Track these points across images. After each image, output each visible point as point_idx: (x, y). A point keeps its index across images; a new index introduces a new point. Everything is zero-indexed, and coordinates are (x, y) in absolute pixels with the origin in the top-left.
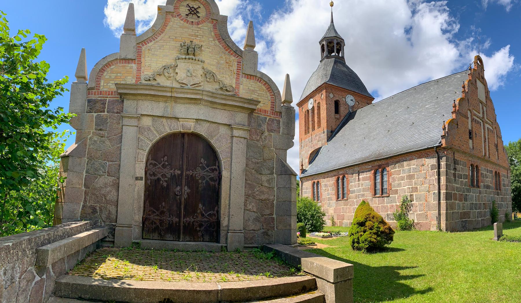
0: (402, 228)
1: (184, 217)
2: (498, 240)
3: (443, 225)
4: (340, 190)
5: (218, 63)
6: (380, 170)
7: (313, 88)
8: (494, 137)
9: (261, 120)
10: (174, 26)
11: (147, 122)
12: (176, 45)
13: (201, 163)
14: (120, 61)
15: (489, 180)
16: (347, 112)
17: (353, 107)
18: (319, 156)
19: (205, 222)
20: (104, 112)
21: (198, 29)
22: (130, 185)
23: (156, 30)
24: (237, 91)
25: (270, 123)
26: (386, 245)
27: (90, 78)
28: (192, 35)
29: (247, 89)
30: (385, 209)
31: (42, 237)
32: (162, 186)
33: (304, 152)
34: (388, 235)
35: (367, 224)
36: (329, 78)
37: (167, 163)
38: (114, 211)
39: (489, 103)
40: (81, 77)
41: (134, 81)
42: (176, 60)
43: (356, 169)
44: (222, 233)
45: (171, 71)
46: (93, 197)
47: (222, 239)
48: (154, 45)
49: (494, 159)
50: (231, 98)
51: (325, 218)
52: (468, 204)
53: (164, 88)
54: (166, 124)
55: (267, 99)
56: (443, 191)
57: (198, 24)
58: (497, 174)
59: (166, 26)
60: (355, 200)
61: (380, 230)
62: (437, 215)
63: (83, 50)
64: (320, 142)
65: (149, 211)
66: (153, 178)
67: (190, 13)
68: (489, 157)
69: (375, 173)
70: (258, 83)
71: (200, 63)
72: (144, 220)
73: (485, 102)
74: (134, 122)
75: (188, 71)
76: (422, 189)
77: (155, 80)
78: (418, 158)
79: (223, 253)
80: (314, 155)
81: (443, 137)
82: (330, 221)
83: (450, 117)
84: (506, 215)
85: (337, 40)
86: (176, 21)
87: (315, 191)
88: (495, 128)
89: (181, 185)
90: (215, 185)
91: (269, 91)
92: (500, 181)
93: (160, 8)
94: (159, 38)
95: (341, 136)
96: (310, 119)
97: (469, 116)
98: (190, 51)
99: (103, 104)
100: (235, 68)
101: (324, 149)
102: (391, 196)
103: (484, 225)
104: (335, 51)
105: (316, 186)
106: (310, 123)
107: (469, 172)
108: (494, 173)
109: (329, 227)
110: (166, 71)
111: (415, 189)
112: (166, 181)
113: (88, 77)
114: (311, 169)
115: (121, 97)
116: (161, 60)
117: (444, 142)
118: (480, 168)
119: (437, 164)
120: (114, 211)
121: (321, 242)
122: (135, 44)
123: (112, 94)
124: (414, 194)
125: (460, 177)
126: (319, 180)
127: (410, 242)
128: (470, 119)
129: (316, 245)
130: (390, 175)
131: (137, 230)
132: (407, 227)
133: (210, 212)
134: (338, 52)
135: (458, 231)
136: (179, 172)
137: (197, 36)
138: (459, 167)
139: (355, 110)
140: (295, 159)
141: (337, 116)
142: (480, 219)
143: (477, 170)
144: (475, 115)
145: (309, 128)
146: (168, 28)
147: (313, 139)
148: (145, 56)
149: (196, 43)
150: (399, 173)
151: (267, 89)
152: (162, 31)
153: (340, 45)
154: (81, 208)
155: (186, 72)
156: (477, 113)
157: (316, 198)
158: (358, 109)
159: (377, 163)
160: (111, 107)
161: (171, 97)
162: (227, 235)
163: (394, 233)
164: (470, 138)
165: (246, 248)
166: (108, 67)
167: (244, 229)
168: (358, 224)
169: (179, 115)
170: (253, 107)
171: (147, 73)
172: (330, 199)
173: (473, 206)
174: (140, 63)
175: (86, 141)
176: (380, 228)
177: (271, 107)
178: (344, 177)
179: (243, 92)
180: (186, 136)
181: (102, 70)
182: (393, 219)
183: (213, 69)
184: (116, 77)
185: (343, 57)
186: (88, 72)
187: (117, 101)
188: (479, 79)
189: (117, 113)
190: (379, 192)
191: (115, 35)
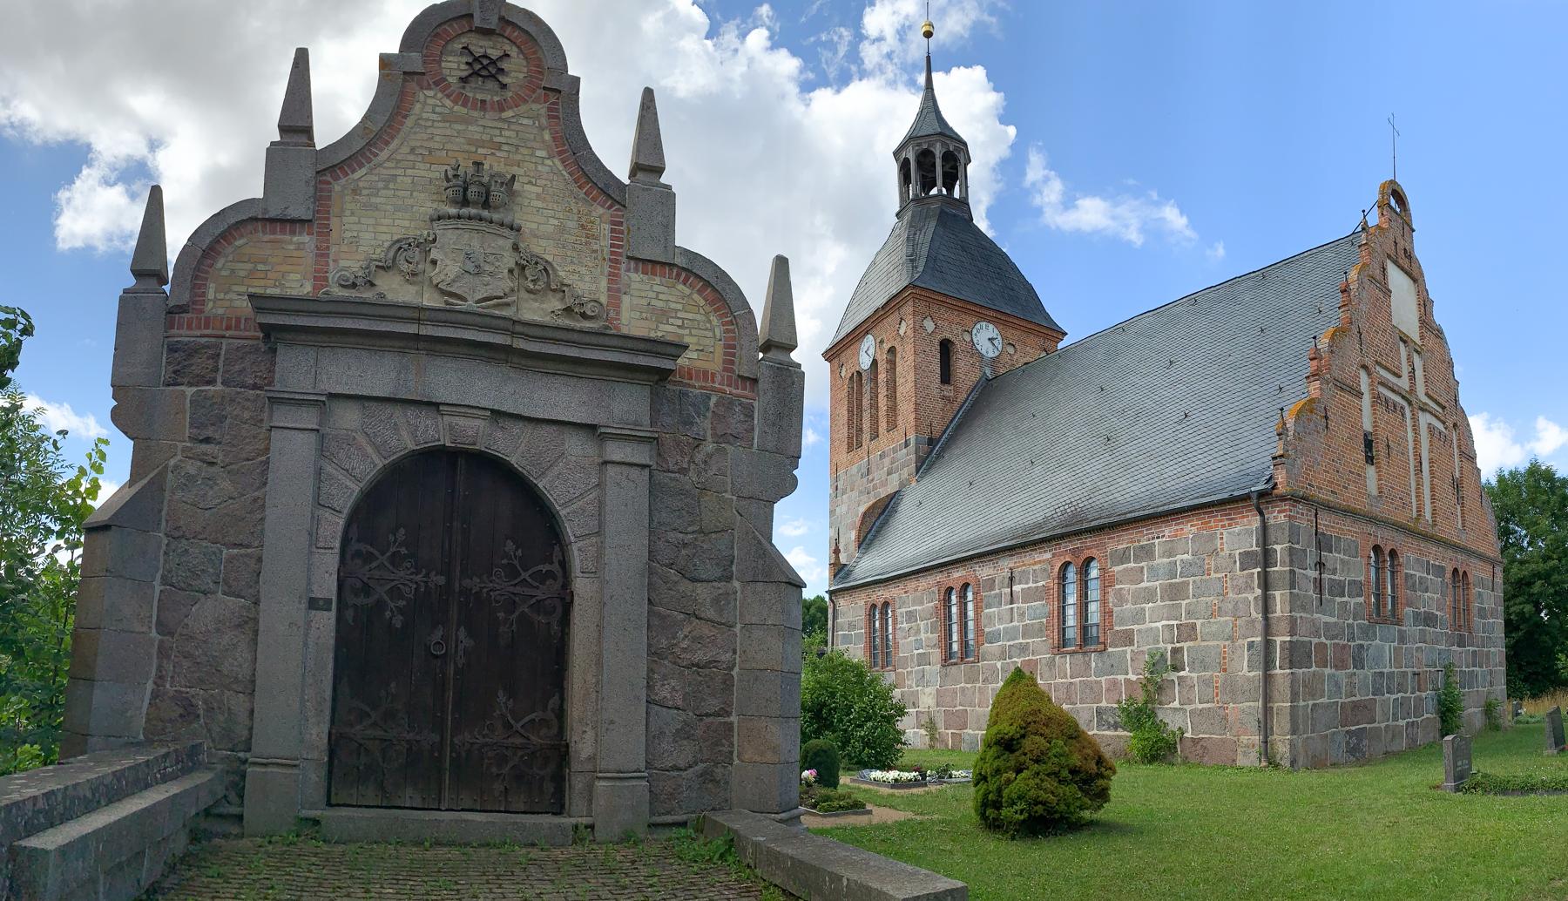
0: (1145, 756)
3: (1282, 746)
5: (562, 229)
8: (1452, 455)
9: (693, 405)
10: (425, 115)
12: (431, 175)
15: (1434, 599)
16: (974, 377)
20: (211, 382)
21: (500, 125)
24: (612, 314)
29: (642, 309)
30: (1093, 691)
31: (29, 805)
33: (844, 508)
34: (1091, 778)
37: (404, 551)
42: (432, 220)
44: (577, 783)
45: (416, 254)
47: (576, 801)
48: (369, 177)
49: (1449, 531)
52: (1366, 677)
57: (502, 110)
59: (405, 117)
60: (999, 665)
62: (1261, 717)
64: (895, 476)
66: (361, 600)
67: (476, 74)
68: (1435, 524)
70: (680, 287)
71: (507, 232)
72: (335, 744)
74: (308, 418)
75: (468, 256)
77: (373, 285)
79: (580, 849)
80: (878, 520)
84: (1489, 710)
85: (943, 144)
86: (430, 101)
88: (1455, 425)
92: (1467, 603)
93: (385, 61)
94: (384, 155)
97: (1364, 388)
98: (476, 197)
104: (939, 181)
107: (1368, 571)
108: (1448, 575)
111: (1188, 632)
112: (400, 610)
114: (869, 566)
122: (310, 173)
123: (237, 327)
124: (1185, 645)
125: (1337, 588)
128: (1367, 400)
131: (313, 776)
133: (533, 716)
136: (441, 580)
137: (499, 146)
138: (1333, 558)
141: (948, 391)
142: (1402, 723)
143: (1392, 566)
146: (409, 122)
147: (874, 468)
148: (343, 210)
149: (496, 169)
150: (1137, 576)
153: (956, 160)
154: (147, 701)
160: (237, 367)
162: (590, 788)
164: (1370, 460)
165: (653, 826)
167: (649, 765)
168: (998, 743)
169: (440, 395)
170: (666, 364)
171: (349, 263)
172: (923, 660)
173: (1382, 683)
174: (325, 232)
175: (162, 475)
177: (725, 361)
179: (632, 321)
180: (461, 462)
182: (1116, 726)
183: (544, 248)
184: (251, 274)
185: (964, 202)
189: (255, 387)
191: (21, 127)
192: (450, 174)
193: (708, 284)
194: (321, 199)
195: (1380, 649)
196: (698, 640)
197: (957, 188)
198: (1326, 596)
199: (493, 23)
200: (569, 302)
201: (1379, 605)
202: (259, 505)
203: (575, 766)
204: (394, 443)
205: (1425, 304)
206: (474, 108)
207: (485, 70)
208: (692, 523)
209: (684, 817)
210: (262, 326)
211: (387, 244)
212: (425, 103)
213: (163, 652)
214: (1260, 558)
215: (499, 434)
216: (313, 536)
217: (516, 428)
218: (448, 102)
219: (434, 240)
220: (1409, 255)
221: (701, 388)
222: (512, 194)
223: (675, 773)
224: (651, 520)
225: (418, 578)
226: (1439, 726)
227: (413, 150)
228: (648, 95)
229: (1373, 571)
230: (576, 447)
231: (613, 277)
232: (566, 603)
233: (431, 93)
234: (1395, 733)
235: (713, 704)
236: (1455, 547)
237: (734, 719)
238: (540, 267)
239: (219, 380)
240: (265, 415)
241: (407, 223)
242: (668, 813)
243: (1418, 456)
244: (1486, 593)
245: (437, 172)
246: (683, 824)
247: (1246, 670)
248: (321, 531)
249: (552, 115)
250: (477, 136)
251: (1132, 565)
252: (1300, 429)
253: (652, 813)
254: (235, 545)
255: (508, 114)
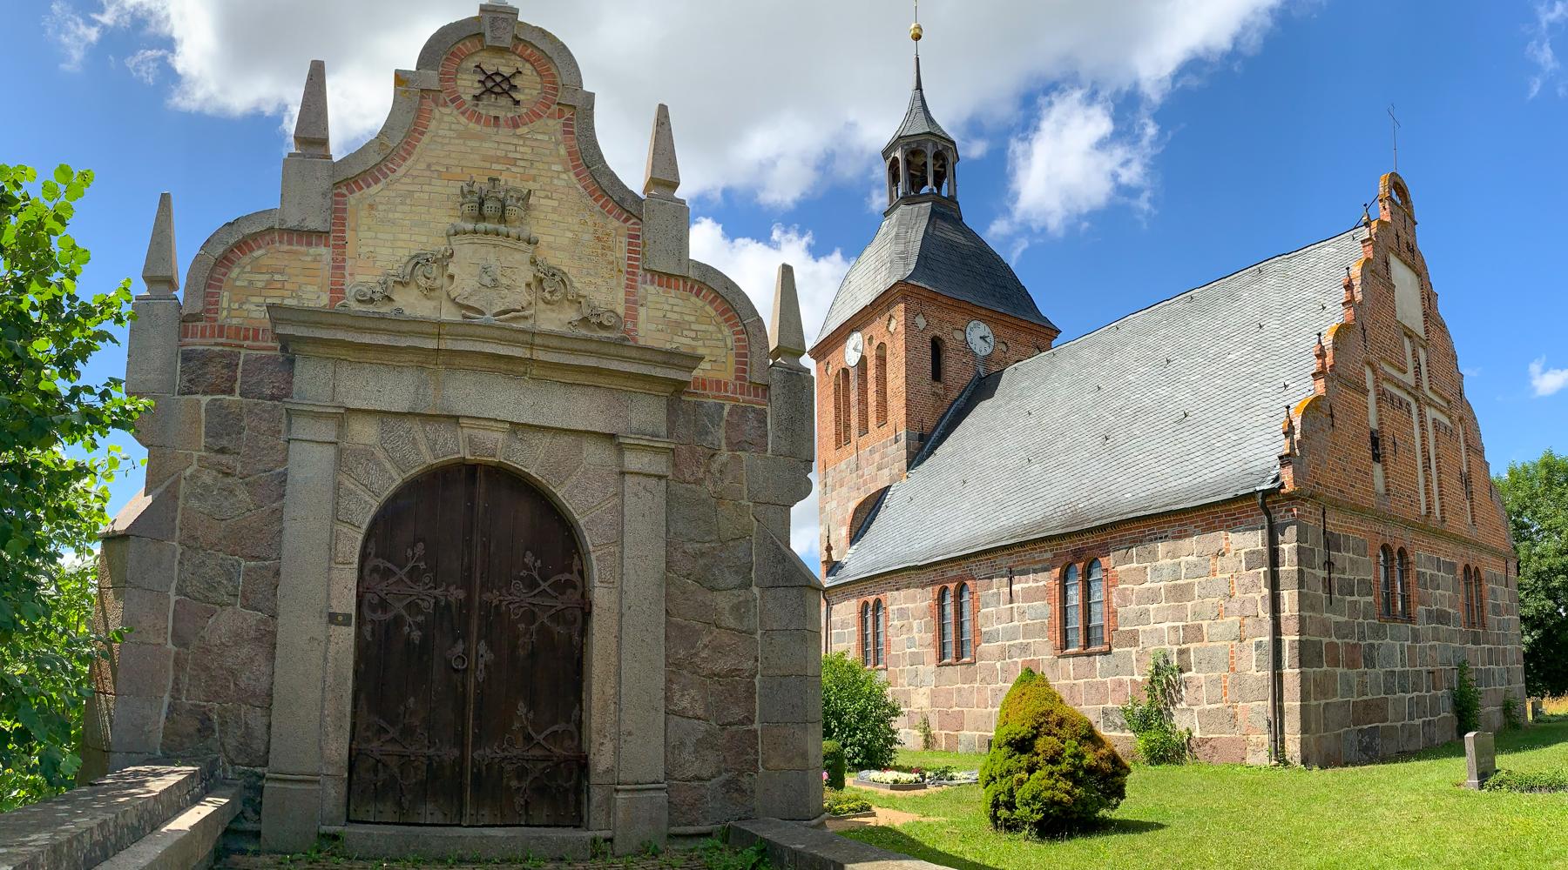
0: (1153, 757)
1: (476, 746)
2: (1481, 787)
3: (1293, 747)
4: (950, 630)
5: (576, 242)
6: (1080, 566)
7: (865, 299)
8: (1459, 450)
10: (441, 132)
11: (365, 433)
13: (526, 567)
14: (281, 237)
15: (1446, 595)
16: (968, 376)
17: (988, 358)
18: (881, 515)
19: (536, 760)
20: (231, 392)
21: (515, 141)
22: (312, 639)
23: (392, 146)
24: (629, 326)
25: (735, 419)
26: (1103, 812)
27: (188, 286)
28: (497, 160)
29: (659, 319)
30: (1100, 692)
32: (408, 642)
33: (834, 504)
34: (1109, 778)
35: (1040, 744)
36: (912, 267)
38: (260, 731)
39: (1436, 337)
40: (160, 279)
41: (324, 300)
43: (1004, 561)
44: (597, 795)
45: (435, 270)
46: (203, 677)
47: (596, 815)
48: (386, 193)
49: (1459, 524)
50: (613, 350)
51: (898, 724)
53: (420, 326)
54: (420, 436)
55: (721, 344)
56: (1290, 638)
57: (516, 126)
58: (1471, 575)
59: (422, 133)
60: (998, 665)
61: (1085, 762)
62: (1270, 715)
63: (165, 199)
64: (886, 471)
65: (367, 729)
66: (379, 616)
67: (489, 91)
69: (1064, 577)
70: (693, 299)
71: (524, 245)
73: (1423, 335)
74: (327, 431)
75: (485, 270)
76: (1219, 633)
77: (390, 299)
78: (1204, 531)
81: (1285, 460)
82: (916, 732)
83: (1306, 389)
84: (1508, 709)
85: (935, 144)
86: (446, 119)
87: (870, 631)
88: (1461, 419)
89: (465, 636)
90: (570, 637)
91: (726, 321)
92: (1481, 599)
93: (401, 78)
94: (401, 171)
95: (953, 454)
96: (854, 397)
97: (1370, 385)
98: (490, 209)
99: (228, 366)
100: (621, 252)
101: (898, 494)
102: (1115, 650)
103: (1432, 740)
104: (930, 180)
105: (872, 613)
106: (854, 412)
107: (1377, 570)
108: (1460, 572)
109: (913, 753)
110: (419, 271)
111: (1194, 633)
112: (419, 626)
113: (182, 281)
114: (858, 561)
115: (284, 349)
116: (406, 237)
117: (1288, 475)
118: (1411, 558)
119: (1265, 550)
120: (260, 731)
121: (891, 804)
122: (326, 184)
124: (1192, 646)
126: (881, 596)
127: (1182, 800)
128: (1372, 396)
129: (874, 815)
130: (1112, 582)
132: (1168, 753)
133: (555, 728)
134: (938, 183)
135: (1346, 765)
136: (461, 594)
138: (1342, 557)
139: (994, 369)
140: (810, 534)
142: (1418, 722)
143: (1401, 564)
144: (1390, 379)
145: (848, 426)
146: (425, 139)
147: (863, 463)
151: (722, 314)
152: (408, 147)
153: (944, 159)
155: (486, 277)
156: (1395, 373)
157: (871, 657)
158: (1007, 365)
159: (1069, 546)
160: (255, 380)
161: (436, 351)
163: (1129, 771)
164: (1376, 457)
165: (673, 837)
166: (244, 254)
167: (668, 776)
168: (1009, 744)
169: (459, 409)
171: (362, 277)
172: (916, 660)
174: (341, 245)
175: (176, 483)
176: (1082, 757)
177: (737, 370)
178: (962, 588)
179: (649, 331)
181: (225, 261)
183: (557, 259)
184: (269, 285)
185: (952, 199)
186: (182, 268)
187: (275, 359)
188: (1398, 255)
189: (273, 397)
190: (1077, 638)
192: (466, 189)
193: (718, 295)
194: (339, 215)
195: (1391, 648)
196: (717, 649)
197: (945, 186)
198: (1336, 595)
199: (507, 42)
200: (586, 312)
201: (1389, 602)
202: (278, 515)
203: (593, 779)
204: (413, 457)
205: (1429, 298)
206: (487, 124)
207: (498, 86)
208: (709, 533)
209: (710, 828)
210: (280, 337)
211: (405, 260)
212: (441, 121)
213: (179, 663)
214: (1266, 557)
215: (518, 446)
216: (332, 547)
217: (536, 439)
218: (463, 120)
219: (452, 255)
220: (1411, 249)
221: (715, 397)
222: (527, 207)
223: (696, 784)
224: (668, 531)
225: (437, 592)
226: (1456, 723)
227: (429, 166)
228: (663, 109)
229: (1382, 569)
230: (594, 454)
231: (631, 288)
232: (586, 611)
233: (447, 110)
234: (1411, 733)
235: (737, 712)
236: (1466, 542)
237: (757, 726)
238: (557, 278)
239: (238, 391)
240: (283, 427)
241: (424, 239)
242: (690, 824)
243: (1425, 451)
244: (1500, 589)
245: (454, 188)
246: (709, 835)
247: (1256, 671)
248: (339, 546)
249: (567, 130)
250: (492, 153)
251: (1135, 565)
252: (1307, 427)
253: (671, 824)
254: (253, 558)
255: (522, 130)
